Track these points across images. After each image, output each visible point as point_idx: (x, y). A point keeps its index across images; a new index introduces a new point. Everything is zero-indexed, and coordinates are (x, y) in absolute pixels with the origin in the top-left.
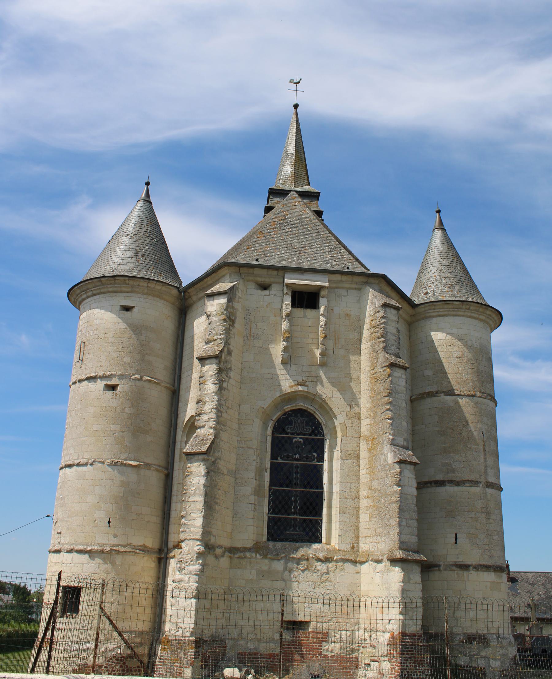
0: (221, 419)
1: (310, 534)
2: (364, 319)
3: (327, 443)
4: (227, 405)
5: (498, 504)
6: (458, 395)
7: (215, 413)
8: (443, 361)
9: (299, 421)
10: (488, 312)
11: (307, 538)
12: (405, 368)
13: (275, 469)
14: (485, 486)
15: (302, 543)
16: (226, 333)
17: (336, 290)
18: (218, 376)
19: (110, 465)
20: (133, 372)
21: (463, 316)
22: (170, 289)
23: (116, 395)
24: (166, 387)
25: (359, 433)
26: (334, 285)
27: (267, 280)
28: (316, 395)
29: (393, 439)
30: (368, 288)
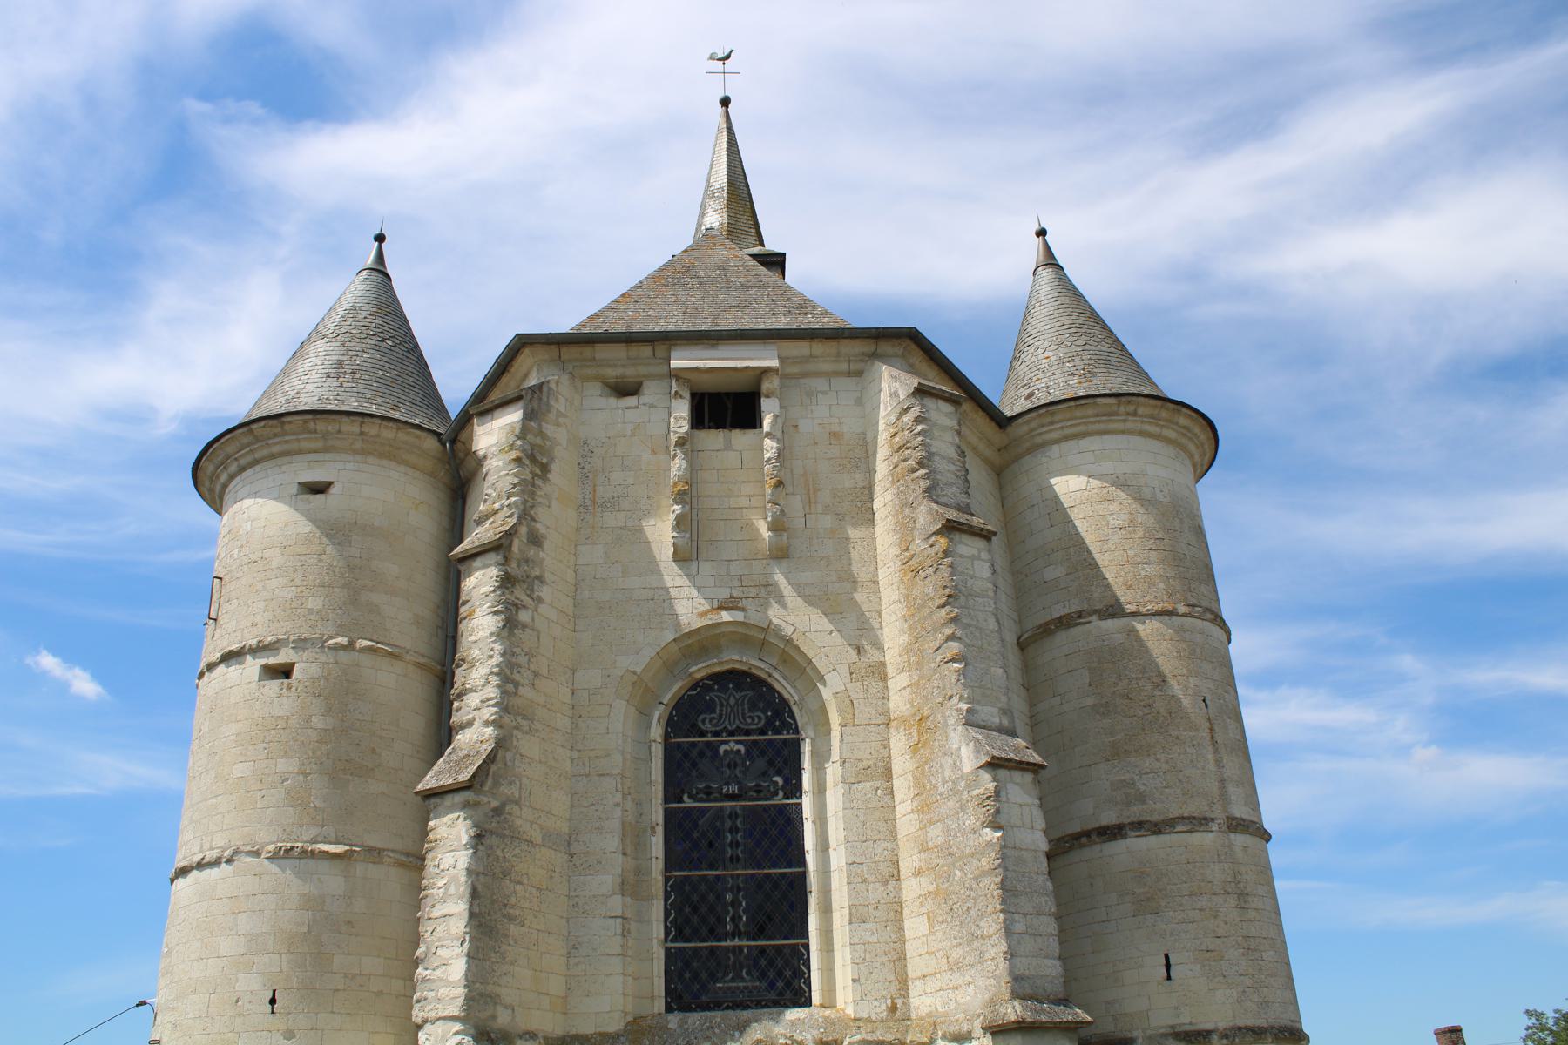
0: (516, 701)
1: (780, 984)
3: (806, 748)
5: (1265, 871)
6: (1134, 614)
7: (498, 686)
9: (732, 701)
10: (1183, 421)
11: (773, 996)
12: (986, 535)
13: (677, 826)
14: (1225, 828)
15: (760, 1011)
16: (523, 492)
17: (802, 381)
18: (503, 594)
19: (274, 857)
20: (329, 629)
21: (1123, 432)
22: (418, 437)
24: (419, 665)
25: (886, 713)
26: (795, 369)
27: (630, 373)
29: (968, 711)
30: (878, 364)
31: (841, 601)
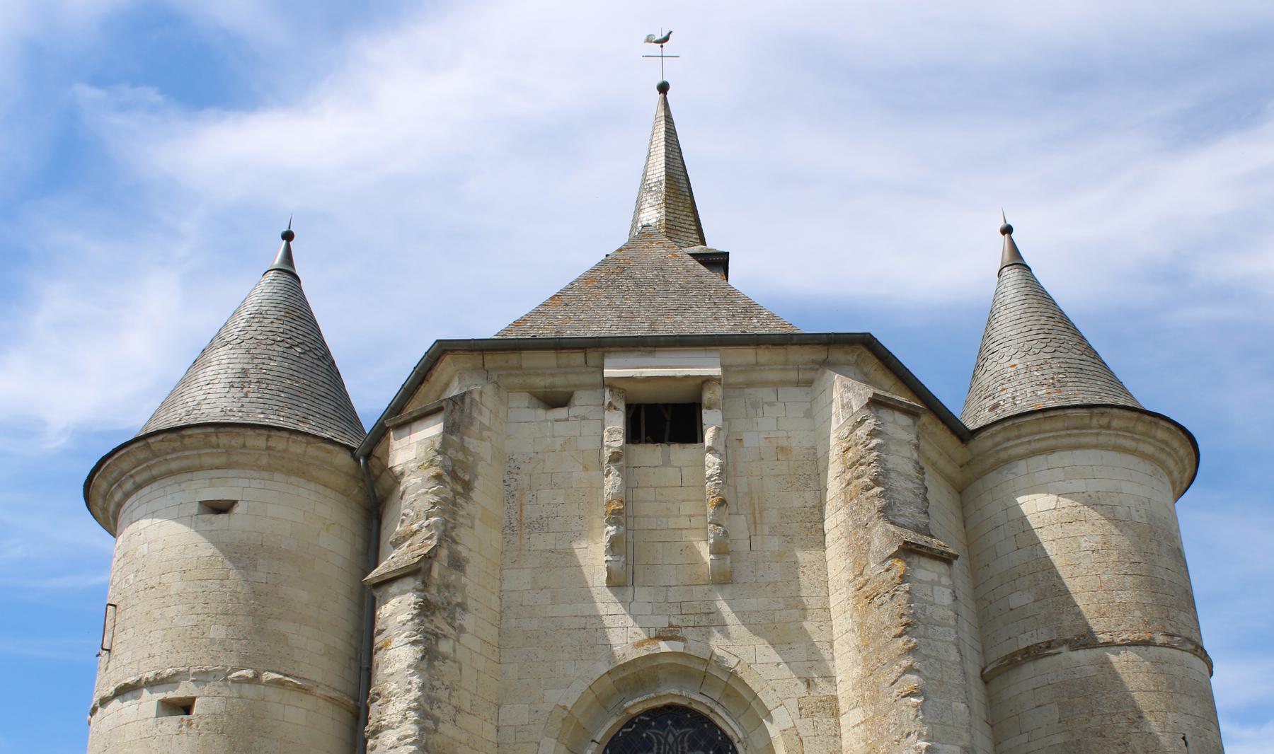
2: (827, 453)
4: (453, 701)
7: (416, 722)
8: (1056, 564)
9: (671, 739)
10: (1160, 434)
12: (946, 559)
16: (443, 511)
17: (747, 391)
18: (422, 623)
20: (233, 661)
21: (1096, 447)
22: (329, 452)
23: (189, 724)
26: (740, 378)
27: (560, 382)
28: (710, 661)
30: (829, 373)
31: (789, 630)
